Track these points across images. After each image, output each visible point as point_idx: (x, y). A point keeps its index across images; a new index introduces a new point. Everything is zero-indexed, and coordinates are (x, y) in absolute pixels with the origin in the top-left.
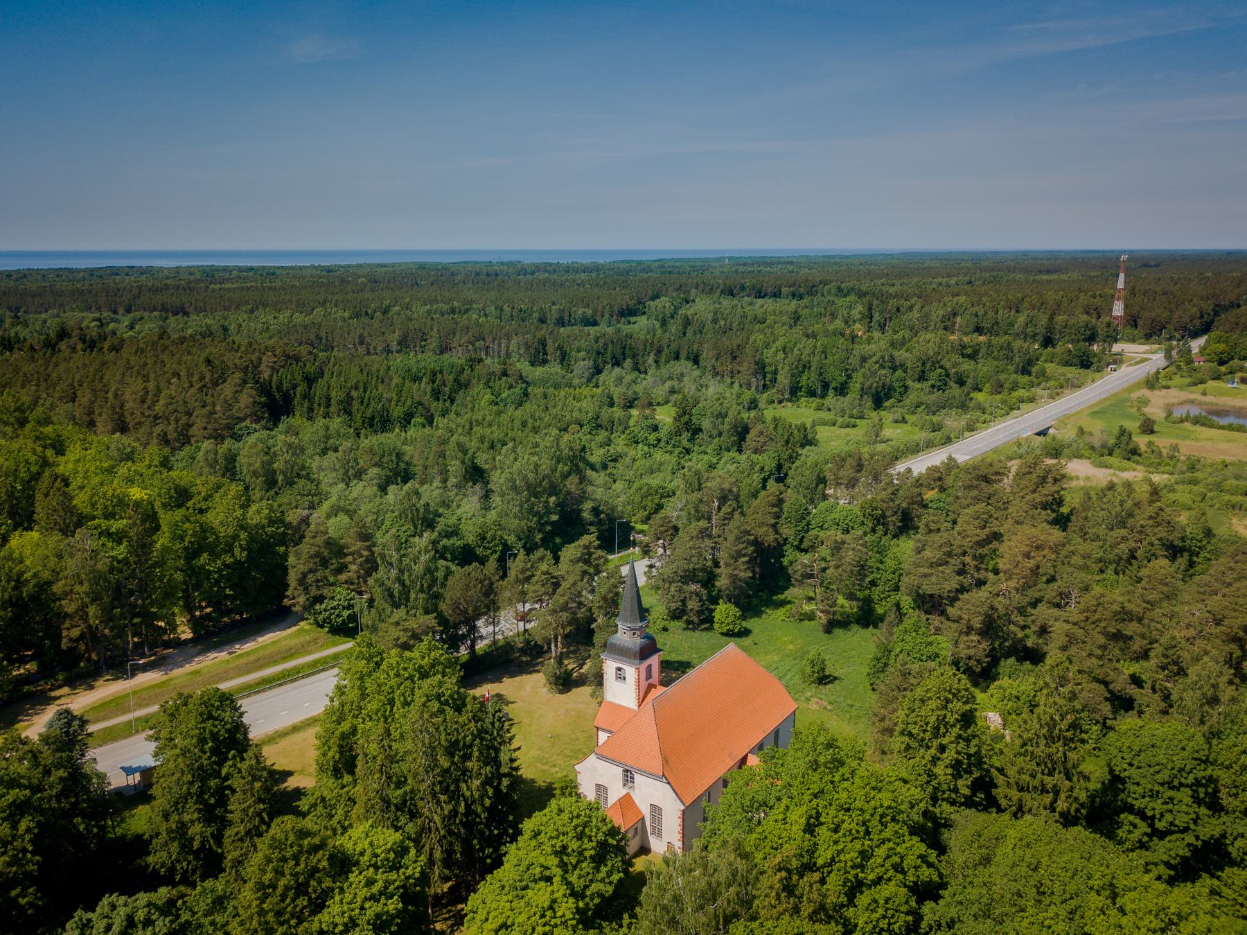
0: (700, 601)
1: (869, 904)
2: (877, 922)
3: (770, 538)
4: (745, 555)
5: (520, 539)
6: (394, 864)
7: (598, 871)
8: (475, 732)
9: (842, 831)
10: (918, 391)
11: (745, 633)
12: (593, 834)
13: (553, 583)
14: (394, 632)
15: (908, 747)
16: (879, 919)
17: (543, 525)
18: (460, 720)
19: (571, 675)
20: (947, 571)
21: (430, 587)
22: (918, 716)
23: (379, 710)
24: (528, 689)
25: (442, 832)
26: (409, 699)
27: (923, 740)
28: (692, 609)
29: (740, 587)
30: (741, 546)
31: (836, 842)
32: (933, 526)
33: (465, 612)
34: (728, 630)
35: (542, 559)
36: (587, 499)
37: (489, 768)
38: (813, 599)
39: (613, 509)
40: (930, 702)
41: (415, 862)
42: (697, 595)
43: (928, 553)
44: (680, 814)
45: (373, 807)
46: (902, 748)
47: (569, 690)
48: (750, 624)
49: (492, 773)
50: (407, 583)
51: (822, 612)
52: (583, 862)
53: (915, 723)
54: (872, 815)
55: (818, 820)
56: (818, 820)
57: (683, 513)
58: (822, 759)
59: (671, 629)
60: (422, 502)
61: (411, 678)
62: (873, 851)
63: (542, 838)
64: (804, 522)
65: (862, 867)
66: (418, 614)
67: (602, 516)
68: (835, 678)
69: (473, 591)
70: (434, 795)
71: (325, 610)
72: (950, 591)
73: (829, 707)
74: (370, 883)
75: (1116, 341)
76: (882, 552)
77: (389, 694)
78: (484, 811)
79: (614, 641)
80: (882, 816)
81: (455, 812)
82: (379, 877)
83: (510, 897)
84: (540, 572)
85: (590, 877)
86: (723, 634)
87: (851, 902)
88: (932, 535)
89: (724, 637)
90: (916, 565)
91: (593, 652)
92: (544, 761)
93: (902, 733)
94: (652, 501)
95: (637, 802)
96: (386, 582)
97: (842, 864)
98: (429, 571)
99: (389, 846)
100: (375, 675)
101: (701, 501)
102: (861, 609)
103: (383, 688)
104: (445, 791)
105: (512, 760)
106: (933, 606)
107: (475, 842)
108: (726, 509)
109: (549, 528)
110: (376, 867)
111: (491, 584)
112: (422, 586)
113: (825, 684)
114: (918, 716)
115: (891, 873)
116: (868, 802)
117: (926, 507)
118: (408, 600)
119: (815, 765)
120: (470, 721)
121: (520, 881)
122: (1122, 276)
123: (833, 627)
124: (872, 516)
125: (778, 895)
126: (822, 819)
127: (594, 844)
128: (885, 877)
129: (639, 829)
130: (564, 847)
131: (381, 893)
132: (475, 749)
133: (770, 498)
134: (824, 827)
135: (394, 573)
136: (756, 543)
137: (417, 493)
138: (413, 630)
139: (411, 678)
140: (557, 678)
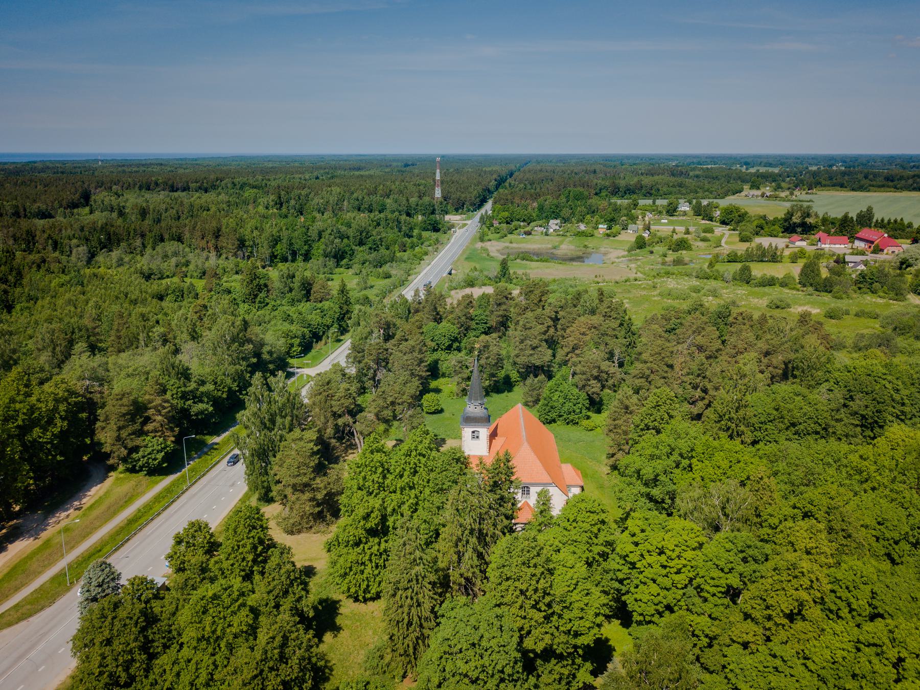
5: (235, 381)
10: (361, 253)
71: (143, 457)
75: (446, 213)
122: (438, 171)
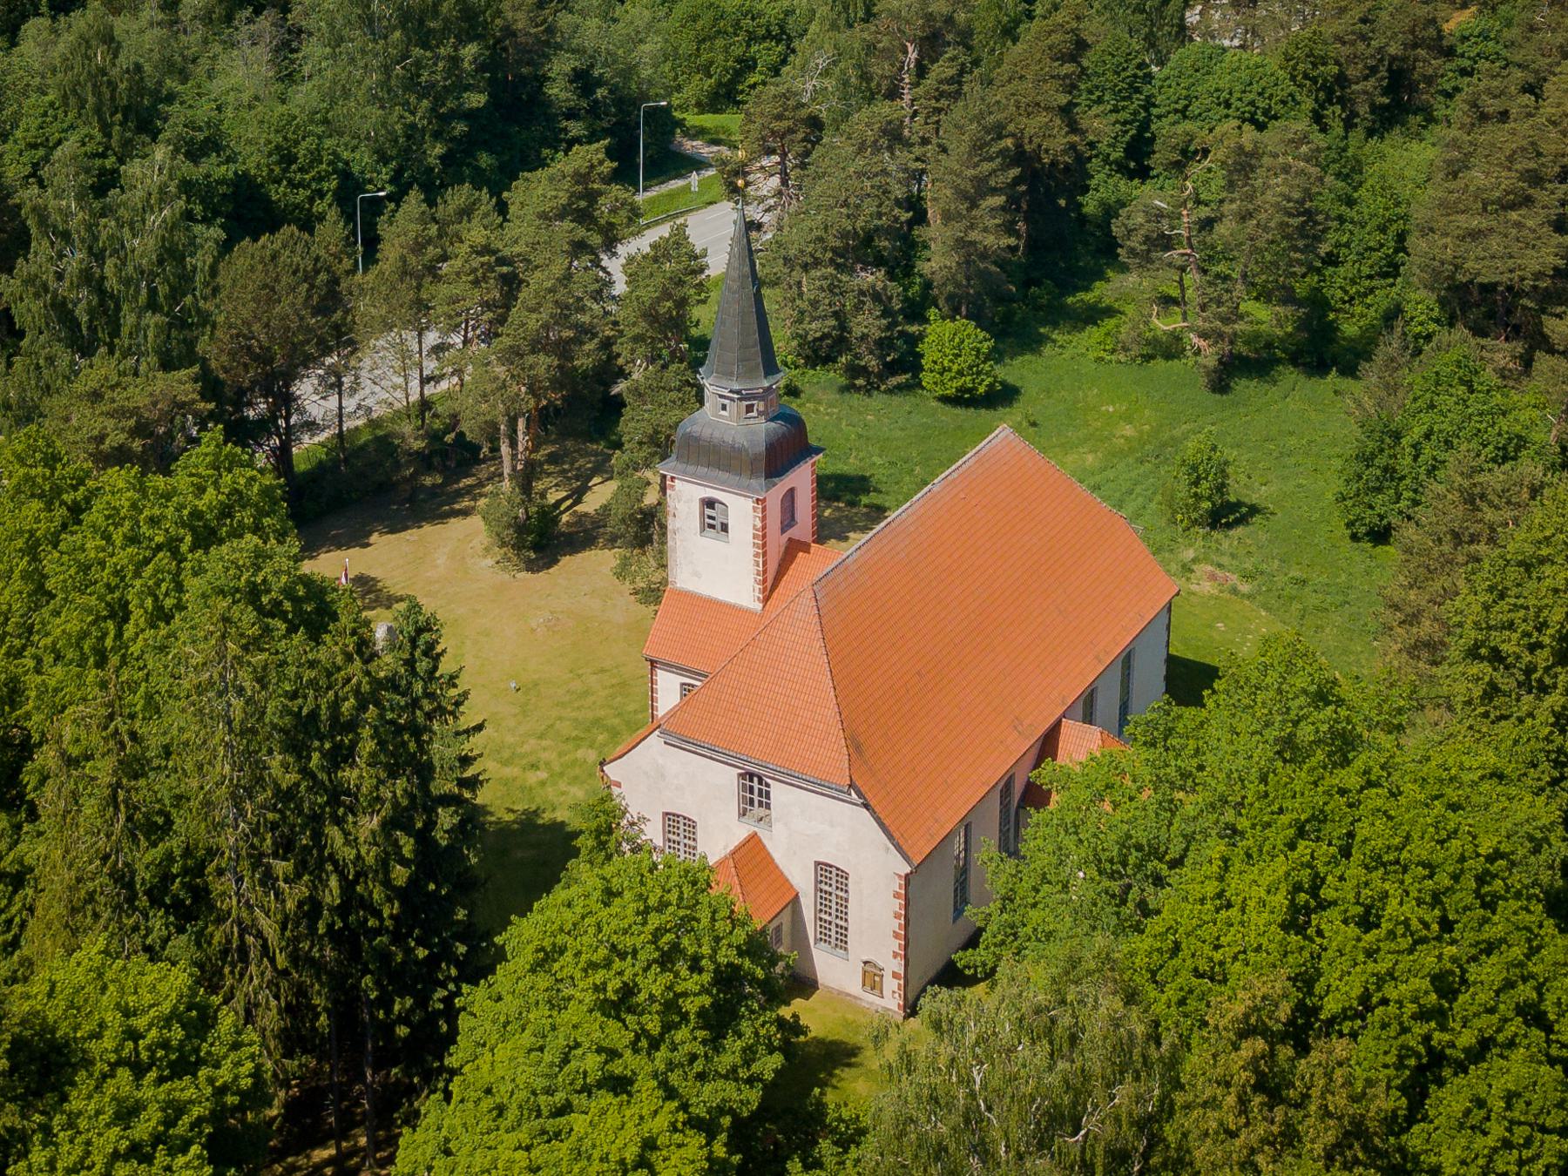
0: (885, 314)
1: (1467, 1113)
2: (1490, 1159)
3: (1057, 143)
4: (994, 191)
5: (384, 159)
6: (183, 1058)
7: (718, 1050)
8: (365, 688)
9: (1386, 925)
11: (1002, 396)
12: (706, 950)
13: (503, 276)
14: (89, 421)
15: (1492, 691)
16: (1495, 1150)
17: (445, 119)
18: (322, 655)
19: (556, 521)
20: (1530, 223)
21: (175, 295)
22: (1516, 608)
23: (84, 635)
24: (441, 561)
25: (282, 961)
26: (169, 602)
27: (1529, 671)
28: (864, 337)
29: (983, 275)
30: (987, 167)
31: (1370, 954)
32: (1491, 105)
33: (265, 358)
34: (960, 390)
35: (466, 212)
36: (559, 47)
37: (401, 783)
38: (1175, 302)
39: (629, 71)
40: (1548, 570)
41: (236, 1046)
42: (876, 297)
43: (1477, 177)
44: (897, 885)
45: (91, 898)
46: (1477, 692)
47: (556, 562)
48: (1012, 371)
49: (412, 797)
50: (112, 284)
51: (1203, 335)
52: (677, 1026)
53: (1511, 626)
54: (1456, 878)
55: (1315, 895)
56: (1315, 895)
57: (830, 83)
58: (1305, 733)
59: (807, 390)
60: (124, 61)
61: (172, 546)
62: (1464, 971)
63: (565, 965)
64: (1138, 100)
65: (1439, 1016)
66: (143, 368)
67: (600, 93)
68: (1254, 510)
69: (286, 302)
70: (257, 860)
72: (1538, 276)
73: (1245, 588)
74: (127, 1113)
76: (1351, 173)
77: (111, 589)
78: (389, 900)
79: (696, 430)
80: (1481, 879)
81: (312, 906)
82: (147, 1093)
83: (523, 1136)
84: (464, 249)
85: (698, 1066)
86: (945, 399)
87: (1416, 1112)
88: (1489, 127)
89: (948, 408)
90: (1448, 208)
91: (618, 459)
92: (506, 754)
93: (1473, 653)
94: (726, 49)
95: (777, 861)
96: (52, 285)
97: (1392, 1009)
98: (171, 254)
99: (166, 1008)
100: (68, 540)
101: (870, 48)
102: (1303, 325)
103: (94, 573)
104: (285, 847)
105: (466, 761)
106: (1491, 315)
107: (367, 980)
108: (941, 70)
109: (460, 128)
110: (139, 1070)
111: (335, 281)
112: (153, 292)
113: (1229, 526)
114: (1516, 608)
115: (1515, 1026)
116: (1441, 842)
117: (1450, 53)
118: (115, 332)
119: (1289, 750)
120: (349, 658)
121: (549, 1091)
123: (1231, 376)
124: (1314, 80)
125: (1243, 1102)
126: (1326, 893)
127: (706, 978)
128: (1500, 1038)
129: (786, 929)
130: (628, 991)
131: (157, 1139)
132: (366, 732)
133: (1056, 38)
134: (1334, 913)
135: (75, 260)
136: (1019, 157)
137: (108, 39)
138: (135, 412)
139: (172, 546)
140: (521, 528)
